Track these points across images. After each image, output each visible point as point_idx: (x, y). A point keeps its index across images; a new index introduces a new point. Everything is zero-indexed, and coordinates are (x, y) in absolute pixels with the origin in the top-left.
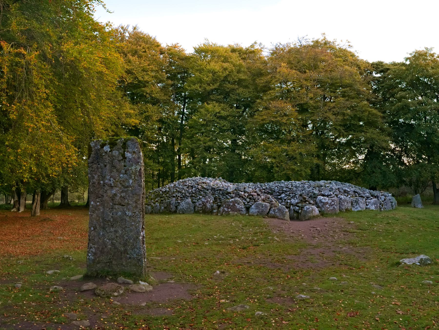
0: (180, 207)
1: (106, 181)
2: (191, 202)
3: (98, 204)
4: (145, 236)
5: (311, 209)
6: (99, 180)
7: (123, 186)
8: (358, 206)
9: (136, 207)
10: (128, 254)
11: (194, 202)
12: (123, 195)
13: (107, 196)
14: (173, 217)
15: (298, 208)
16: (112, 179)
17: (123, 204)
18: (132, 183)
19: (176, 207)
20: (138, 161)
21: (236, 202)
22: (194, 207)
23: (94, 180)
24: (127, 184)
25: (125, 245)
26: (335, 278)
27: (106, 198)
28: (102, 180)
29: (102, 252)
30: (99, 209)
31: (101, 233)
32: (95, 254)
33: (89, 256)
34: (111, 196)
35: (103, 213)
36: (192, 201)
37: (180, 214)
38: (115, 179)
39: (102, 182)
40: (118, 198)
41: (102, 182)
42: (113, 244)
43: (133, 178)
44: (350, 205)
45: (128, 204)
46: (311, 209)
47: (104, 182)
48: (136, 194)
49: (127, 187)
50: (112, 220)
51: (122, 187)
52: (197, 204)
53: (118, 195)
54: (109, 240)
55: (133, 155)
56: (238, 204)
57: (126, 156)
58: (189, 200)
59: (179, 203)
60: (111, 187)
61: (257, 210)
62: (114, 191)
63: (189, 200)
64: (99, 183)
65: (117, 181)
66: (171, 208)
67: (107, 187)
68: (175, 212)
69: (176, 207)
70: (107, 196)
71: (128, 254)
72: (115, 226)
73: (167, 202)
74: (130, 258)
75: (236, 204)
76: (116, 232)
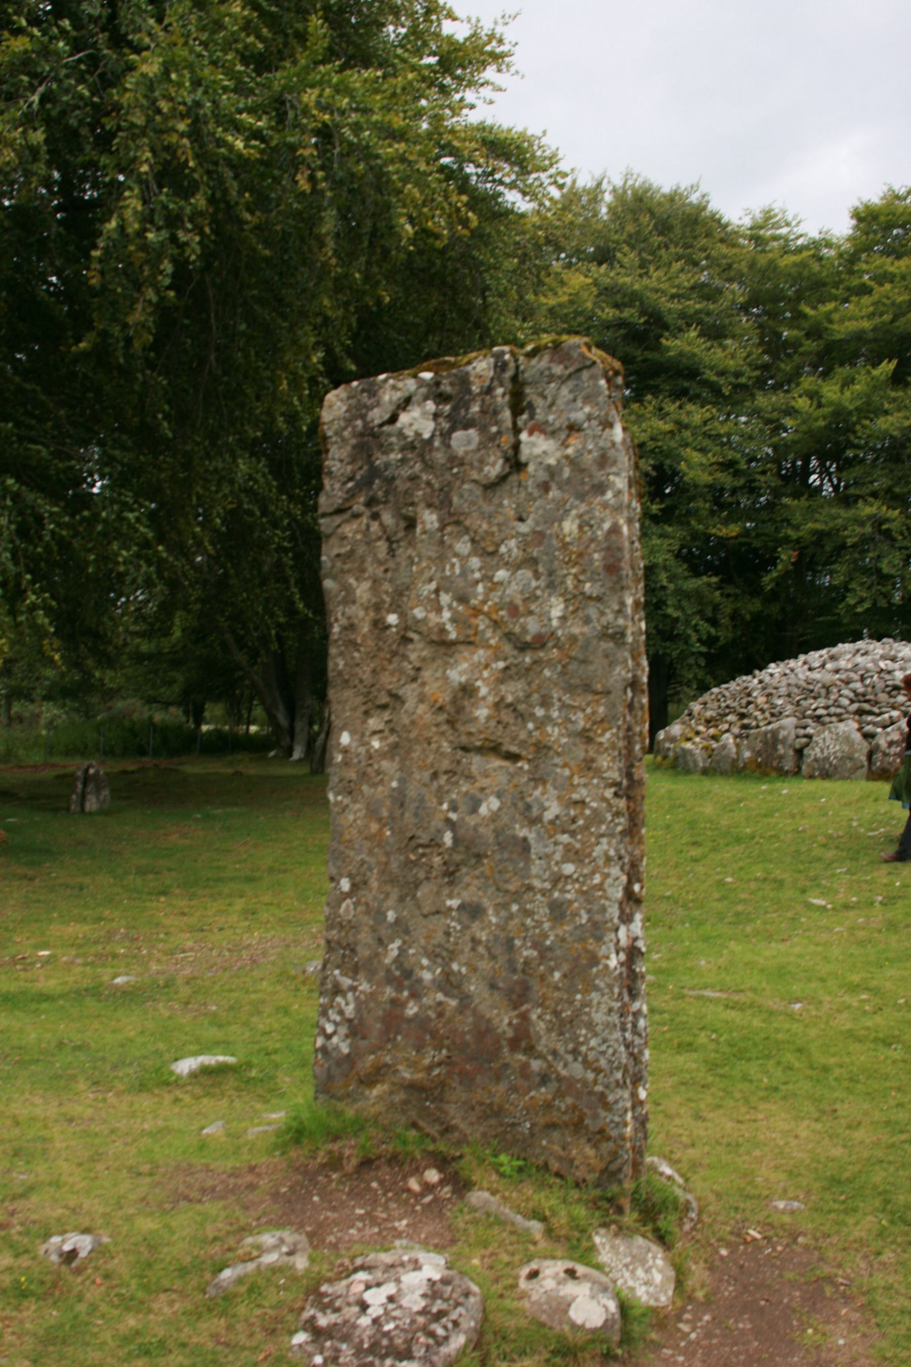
0: (814, 753)
1: (419, 613)
2: (857, 736)
3: (376, 744)
4: (640, 944)
6: (378, 607)
7: (509, 636)
10: (530, 1050)
11: (868, 736)
12: (512, 691)
13: (422, 699)
14: (786, 788)
16: (445, 598)
17: (514, 749)
18: (563, 618)
20: (599, 476)
22: (870, 755)
23: (352, 610)
24: (533, 626)
25: (518, 996)
28: (396, 607)
30: (380, 777)
31: (391, 916)
32: (355, 1029)
33: (329, 1037)
34: (444, 698)
35: (399, 799)
36: (860, 729)
37: (811, 777)
38: (462, 599)
39: (392, 619)
41: (392, 619)
43: (570, 582)
45: (542, 748)
47: (403, 615)
48: (587, 688)
49: (540, 642)
50: (448, 838)
51: (507, 648)
52: (882, 742)
53: (483, 691)
54: (433, 956)
55: (565, 445)
57: (525, 453)
58: (850, 726)
59: (809, 737)
60: (443, 646)
62: (457, 675)
63: (850, 726)
64: (379, 625)
65: (477, 612)
66: (781, 757)
67: (416, 652)
68: (797, 772)
69: (799, 752)
70: (422, 699)
71: (530, 1050)
73: (766, 733)
74: (544, 1079)
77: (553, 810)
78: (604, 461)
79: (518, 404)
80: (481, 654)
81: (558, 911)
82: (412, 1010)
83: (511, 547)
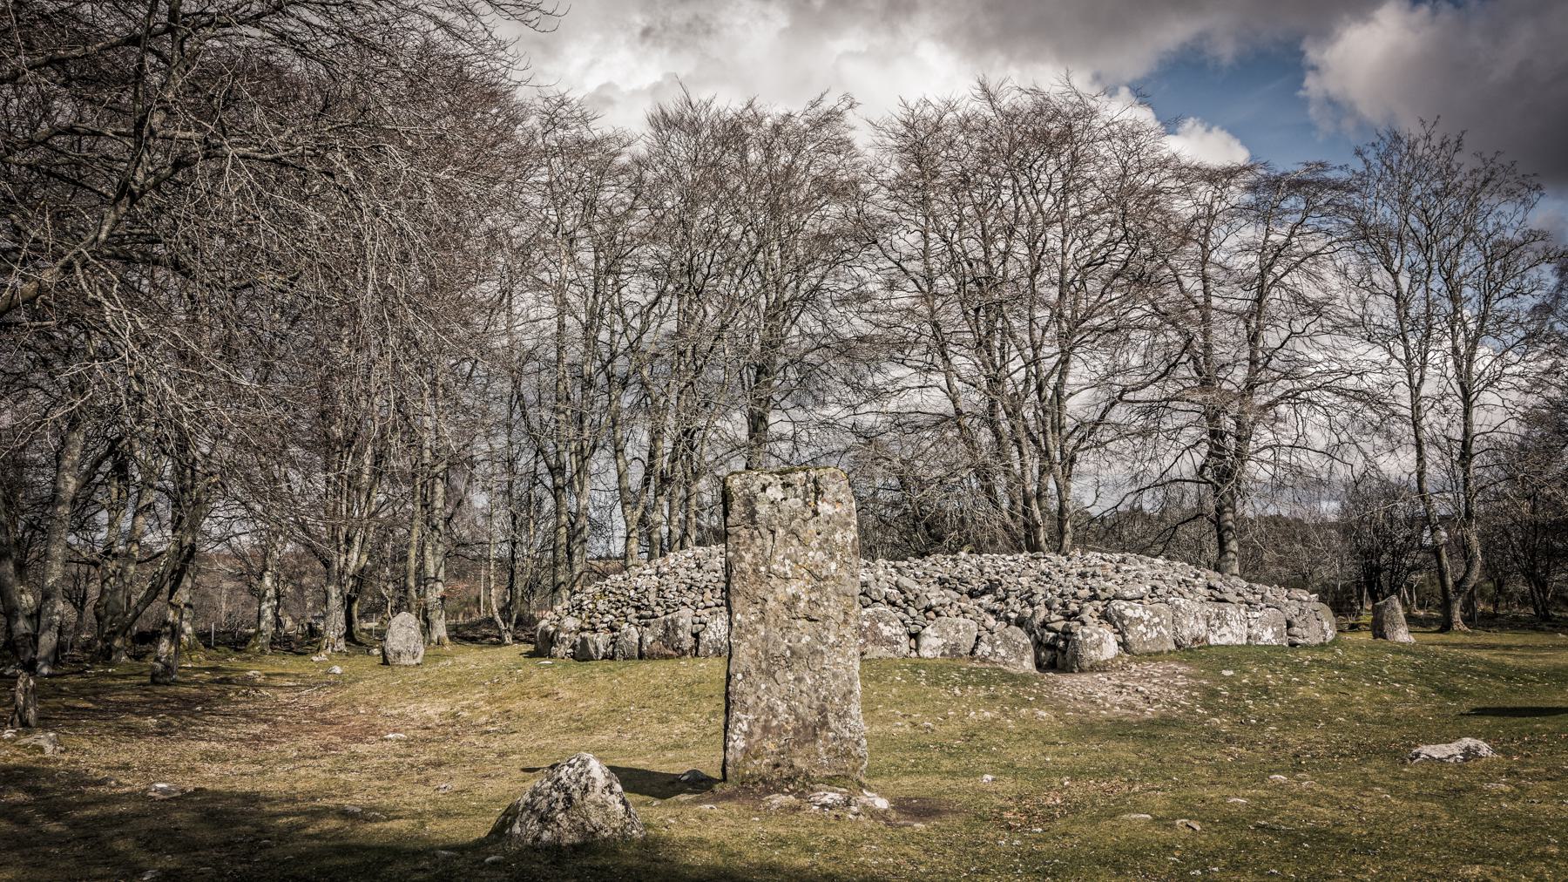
0: (706, 637)
1: (775, 567)
5: (1096, 636)
8: (1225, 629)
9: (845, 621)
10: (829, 729)
15: (1051, 634)
19: (696, 636)
21: (879, 618)
23: (743, 565)
24: (824, 573)
26: (1437, 751)
27: (771, 604)
29: (766, 729)
30: (756, 631)
35: (766, 639)
40: (802, 604)
42: (792, 710)
44: (1203, 625)
45: (827, 617)
46: (1096, 636)
50: (788, 653)
56: (887, 624)
61: (940, 642)
64: (756, 571)
66: (681, 640)
67: (774, 581)
69: (696, 636)
71: (829, 729)
72: (796, 667)
75: (881, 625)
76: (799, 680)
77: (832, 639)
78: (849, 515)
79: (818, 492)
80: (802, 583)
81: (835, 676)
82: (774, 723)
83: (814, 543)
